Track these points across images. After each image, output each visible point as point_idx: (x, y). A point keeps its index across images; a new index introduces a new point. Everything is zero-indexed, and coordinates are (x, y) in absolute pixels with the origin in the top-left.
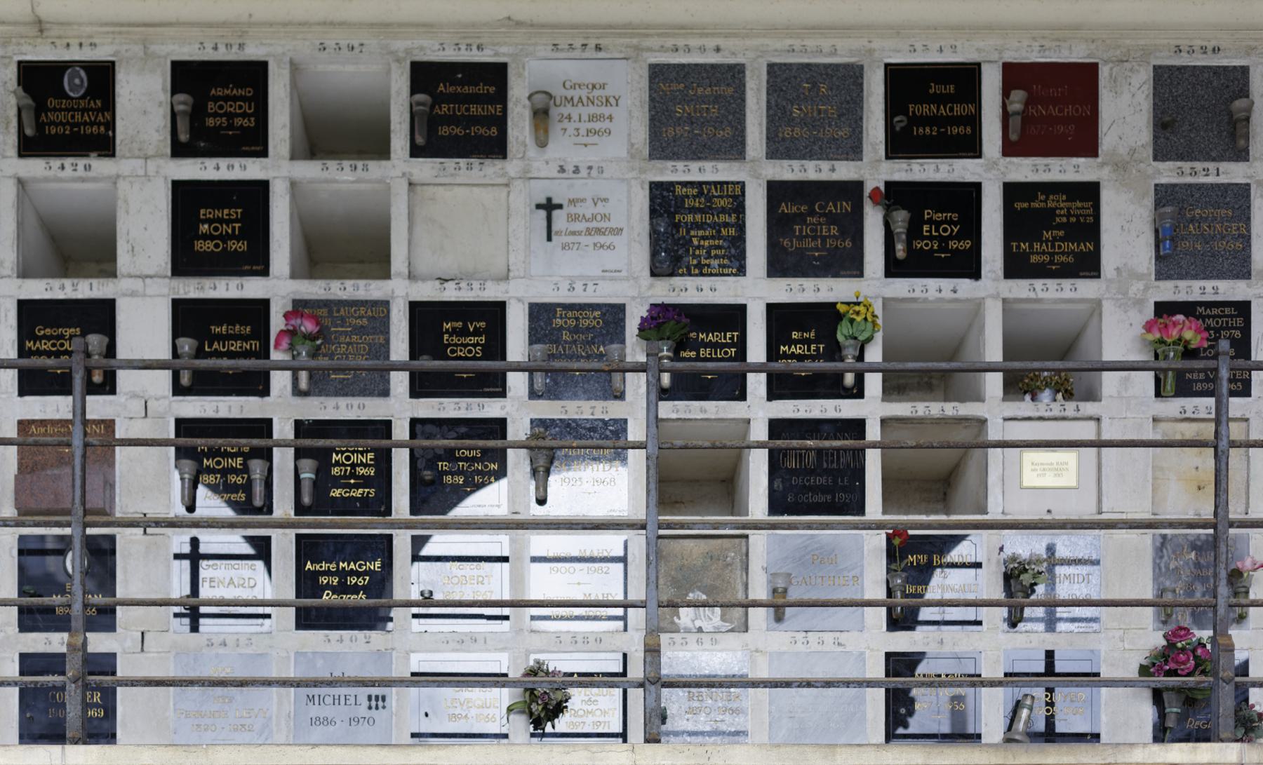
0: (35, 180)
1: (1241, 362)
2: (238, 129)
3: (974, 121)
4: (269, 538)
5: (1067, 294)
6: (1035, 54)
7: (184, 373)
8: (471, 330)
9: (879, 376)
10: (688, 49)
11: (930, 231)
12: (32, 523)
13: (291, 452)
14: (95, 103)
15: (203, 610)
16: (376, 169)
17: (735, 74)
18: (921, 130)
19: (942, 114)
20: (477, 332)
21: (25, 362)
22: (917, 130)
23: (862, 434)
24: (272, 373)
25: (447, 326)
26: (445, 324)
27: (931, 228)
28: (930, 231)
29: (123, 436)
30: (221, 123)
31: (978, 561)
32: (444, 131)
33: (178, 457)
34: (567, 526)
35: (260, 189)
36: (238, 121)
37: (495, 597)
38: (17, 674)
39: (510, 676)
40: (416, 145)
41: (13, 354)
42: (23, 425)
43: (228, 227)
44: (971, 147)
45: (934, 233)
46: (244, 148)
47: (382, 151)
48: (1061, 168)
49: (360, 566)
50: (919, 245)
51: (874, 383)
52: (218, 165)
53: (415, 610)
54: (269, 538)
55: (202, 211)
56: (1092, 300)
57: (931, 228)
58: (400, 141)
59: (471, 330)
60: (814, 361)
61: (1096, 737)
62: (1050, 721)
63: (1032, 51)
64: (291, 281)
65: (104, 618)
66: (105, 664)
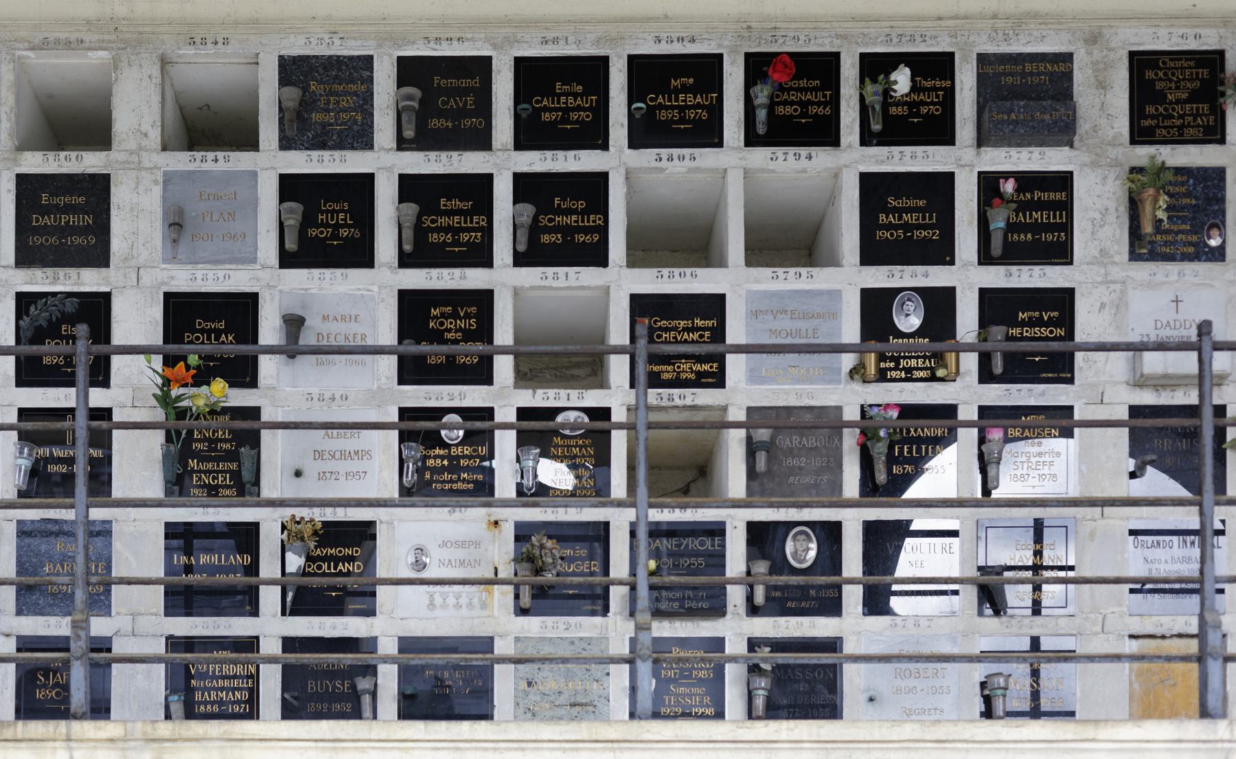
0: (640, 170)
1: (100, 349)
2: (810, 117)
3: (717, 110)
4: (256, 525)
5: (572, 282)
6: (828, 47)
7: (951, 356)
8: (1046, 318)
9: (510, 358)
10: (555, 41)
11: (345, 220)
12: (520, 504)
13: (512, 435)
14: (1025, 196)
15: (1029, 574)
16: (707, 157)
17: (482, 66)
18: (1015, 236)
19: (1021, 221)
20: (468, 316)
21: (292, 657)
22: (1012, 237)
23: (94, 384)
24: (495, 357)
25: (434, 312)
26: (1020, 314)
27: (346, 216)
28: (345, 220)
29: (972, 429)
30: (673, 116)
31: (1133, 537)
32: (435, 123)
33: (520, 444)
34: (1061, 504)
35: (601, 180)
36: (813, 110)
37: (945, 574)
38: (396, 652)
39: (1077, 651)
40: (403, 138)
41: (11, 341)
42: (405, 413)
43: (567, 218)
44: (362, 139)
45: (349, 222)
46: (703, 380)
47: (250, 142)
48: (772, 156)
49: (340, 552)
50: (313, 232)
51: (504, 367)
52: (810, 154)
53: (1071, 574)
54: (256, 525)
55: (443, 201)
56: (602, 286)
57: (346, 216)
58: (269, 132)
59: (1046, 318)
60: (433, 344)
61: (1072, 714)
62: (1035, 695)
63: (429, 42)
64: (629, 270)
65: (100, 602)
66: (102, 646)
